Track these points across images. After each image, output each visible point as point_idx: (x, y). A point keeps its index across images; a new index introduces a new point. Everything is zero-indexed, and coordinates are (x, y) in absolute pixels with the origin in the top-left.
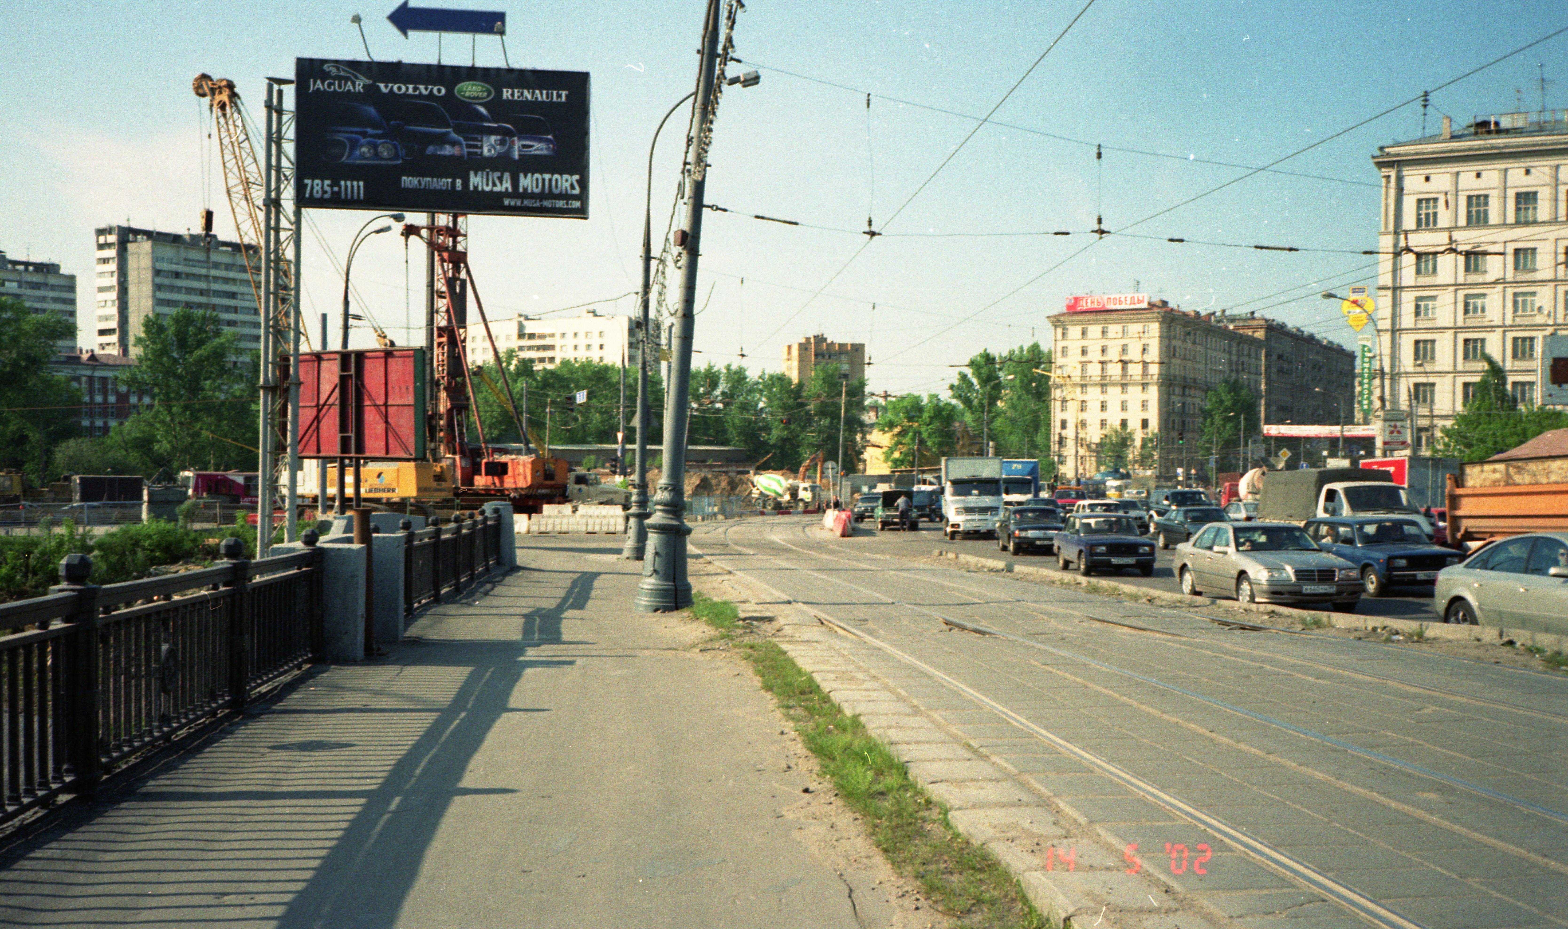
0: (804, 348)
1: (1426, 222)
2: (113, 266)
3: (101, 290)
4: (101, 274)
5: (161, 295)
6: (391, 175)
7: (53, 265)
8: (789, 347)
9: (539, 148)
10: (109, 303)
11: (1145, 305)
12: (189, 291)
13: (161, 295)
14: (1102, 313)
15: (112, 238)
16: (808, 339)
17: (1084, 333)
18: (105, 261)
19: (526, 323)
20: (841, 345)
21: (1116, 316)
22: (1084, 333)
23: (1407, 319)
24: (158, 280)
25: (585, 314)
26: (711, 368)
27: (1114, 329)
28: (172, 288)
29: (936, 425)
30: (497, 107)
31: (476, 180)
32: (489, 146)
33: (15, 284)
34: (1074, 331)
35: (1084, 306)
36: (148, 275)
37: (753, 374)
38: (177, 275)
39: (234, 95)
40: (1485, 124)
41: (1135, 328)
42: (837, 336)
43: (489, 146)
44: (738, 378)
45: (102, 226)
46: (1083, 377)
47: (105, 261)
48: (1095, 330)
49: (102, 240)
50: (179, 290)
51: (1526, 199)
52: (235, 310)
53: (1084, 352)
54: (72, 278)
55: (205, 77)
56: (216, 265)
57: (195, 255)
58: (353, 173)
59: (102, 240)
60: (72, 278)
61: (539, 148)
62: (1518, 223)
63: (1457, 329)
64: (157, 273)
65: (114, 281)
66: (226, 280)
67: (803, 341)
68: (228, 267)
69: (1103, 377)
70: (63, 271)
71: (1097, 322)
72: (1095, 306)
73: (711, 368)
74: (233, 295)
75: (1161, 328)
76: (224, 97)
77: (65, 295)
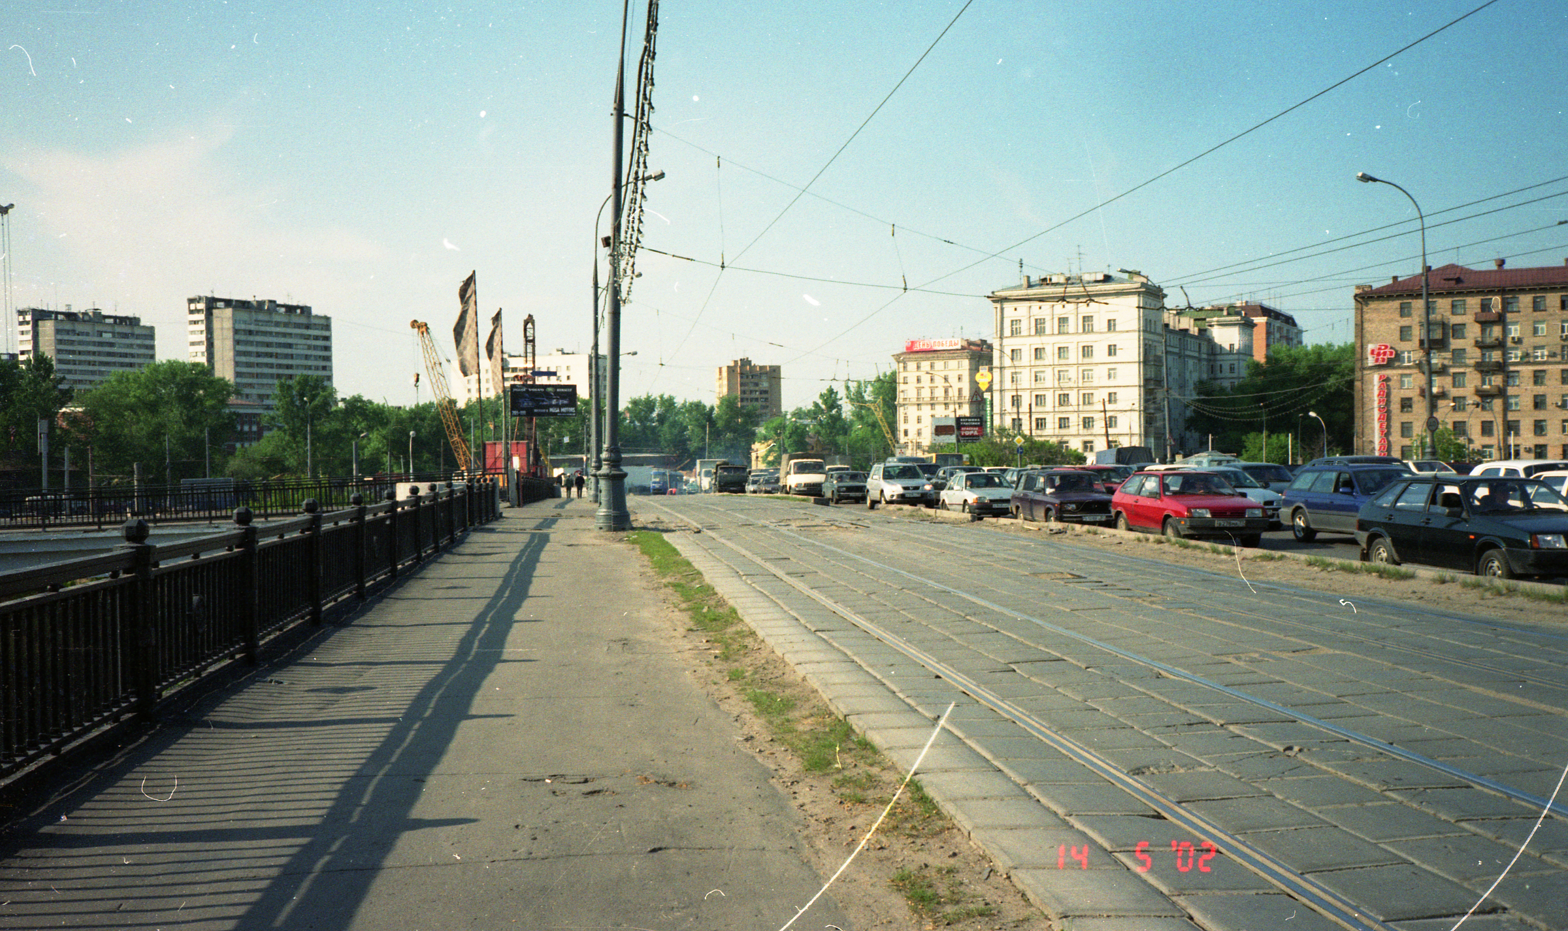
0: (731, 370)
1: (1015, 333)
2: (202, 327)
3: (193, 344)
4: (192, 332)
5: (241, 348)
6: (532, 409)
7: (135, 318)
8: (720, 369)
9: (565, 402)
10: (199, 354)
11: (959, 347)
12: (258, 344)
13: (241, 348)
14: (931, 353)
15: (201, 306)
16: (736, 362)
17: (918, 367)
18: (195, 322)
19: (509, 359)
20: (761, 368)
21: (939, 354)
22: (918, 367)
23: (1008, 384)
24: (237, 337)
25: (555, 352)
26: (649, 397)
27: (939, 364)
28: (247, 343)
29: (794, 437)
30: (556, 393)
31: (551, 410)
32: (554, 402)
33: (110, 335)
34: (912, 365)
35: (917, 347)
36: (230, 334)
37: (679, 401)
38: (250, 332)
39: (427, 329)
40: (1044, 280)
41: (953, 364)
42: (761, 359)
43: (554, 402)
44: (669, 403)
45: (192, 296)
46: (918, 399)
47: (195, 322)
48: (925, 365)
49: (193, 307)
50: (251, 343)
51: (1063, 321)
52: (291, 356)
53: (919, 380)
54: (152, 329)
55: (415, 321)
56: (277, 324)
57: (261, 317)
58: (523, 409)
59: (193, 307)
60: (152, 329)
61: (565, 402)
62: (1060, 333)
63: (1032, 390)
64: (236, 331)
65: (203, 337)
66: (284, 335)
67: (732, 364)
68: (286, 325)
69: (932, 398)
70: (142, 323)
71: (927, 359)
72: (925, 347)
73: (649, 397)
74: (290, 346)
75: (970, 364)
76: (424, 329)
77: (148, 342)
